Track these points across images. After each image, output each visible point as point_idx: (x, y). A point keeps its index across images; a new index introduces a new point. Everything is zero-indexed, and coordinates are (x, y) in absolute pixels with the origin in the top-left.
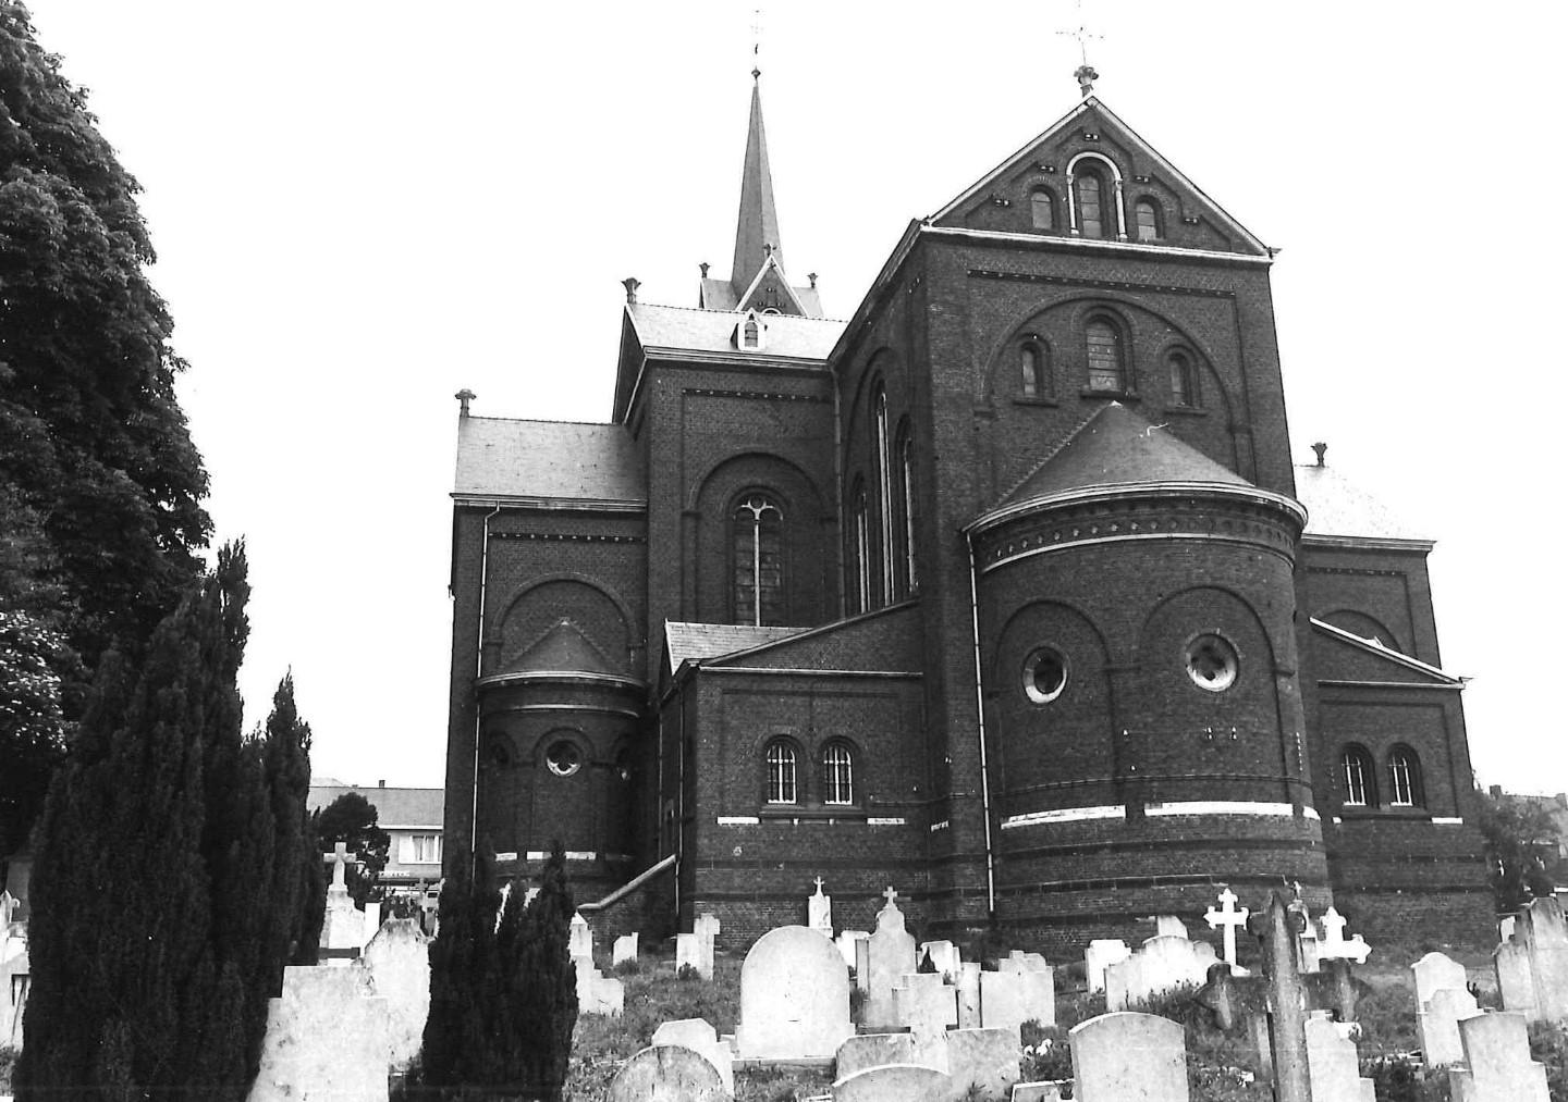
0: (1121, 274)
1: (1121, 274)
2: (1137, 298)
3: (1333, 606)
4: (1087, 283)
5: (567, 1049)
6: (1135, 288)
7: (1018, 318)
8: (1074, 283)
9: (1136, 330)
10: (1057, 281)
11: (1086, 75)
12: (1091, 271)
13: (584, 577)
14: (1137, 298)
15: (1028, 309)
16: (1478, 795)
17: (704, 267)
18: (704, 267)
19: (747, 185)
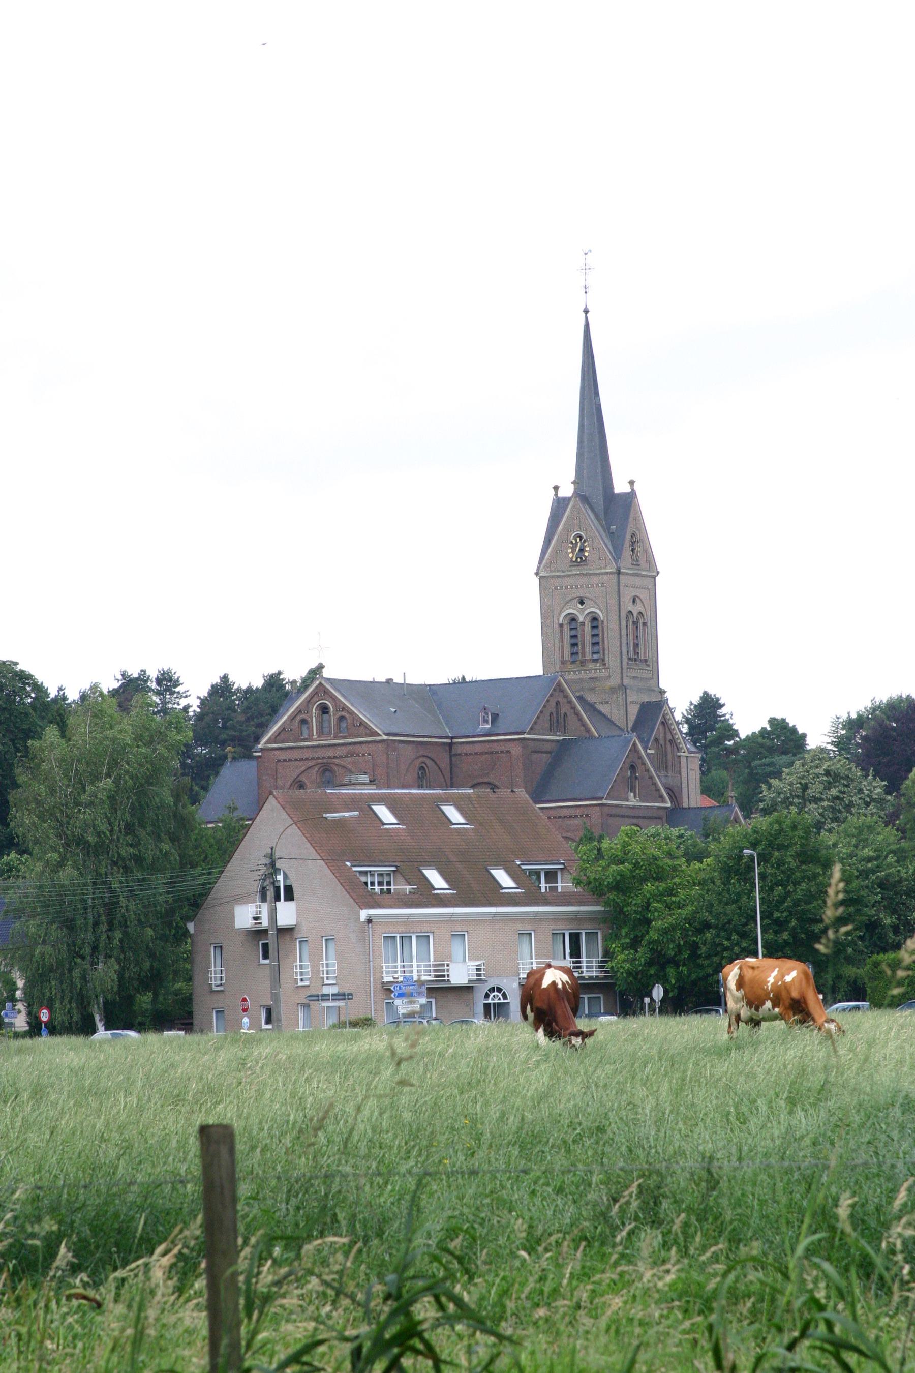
0: (330, 753)
1: (330, 753)
2: (337, 761)
3: (475, 782)
4: (318, 758)
5: (234, 1200)
6: (335, 757)
7: (295, 775)
8: (313, 759)
9: (337, 774)
10: (307, 759)
11: (632, 483)
12: (320, 753)
13: (481, 780)
14: (337, 761)
15: (298, 772)
16: (654, 709)
17: (556, 488)
18: (556, 488)
19: (586, 422)
